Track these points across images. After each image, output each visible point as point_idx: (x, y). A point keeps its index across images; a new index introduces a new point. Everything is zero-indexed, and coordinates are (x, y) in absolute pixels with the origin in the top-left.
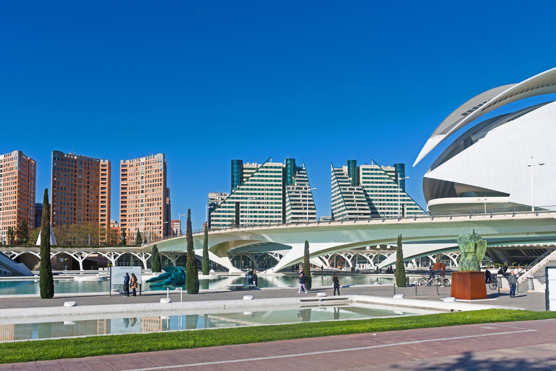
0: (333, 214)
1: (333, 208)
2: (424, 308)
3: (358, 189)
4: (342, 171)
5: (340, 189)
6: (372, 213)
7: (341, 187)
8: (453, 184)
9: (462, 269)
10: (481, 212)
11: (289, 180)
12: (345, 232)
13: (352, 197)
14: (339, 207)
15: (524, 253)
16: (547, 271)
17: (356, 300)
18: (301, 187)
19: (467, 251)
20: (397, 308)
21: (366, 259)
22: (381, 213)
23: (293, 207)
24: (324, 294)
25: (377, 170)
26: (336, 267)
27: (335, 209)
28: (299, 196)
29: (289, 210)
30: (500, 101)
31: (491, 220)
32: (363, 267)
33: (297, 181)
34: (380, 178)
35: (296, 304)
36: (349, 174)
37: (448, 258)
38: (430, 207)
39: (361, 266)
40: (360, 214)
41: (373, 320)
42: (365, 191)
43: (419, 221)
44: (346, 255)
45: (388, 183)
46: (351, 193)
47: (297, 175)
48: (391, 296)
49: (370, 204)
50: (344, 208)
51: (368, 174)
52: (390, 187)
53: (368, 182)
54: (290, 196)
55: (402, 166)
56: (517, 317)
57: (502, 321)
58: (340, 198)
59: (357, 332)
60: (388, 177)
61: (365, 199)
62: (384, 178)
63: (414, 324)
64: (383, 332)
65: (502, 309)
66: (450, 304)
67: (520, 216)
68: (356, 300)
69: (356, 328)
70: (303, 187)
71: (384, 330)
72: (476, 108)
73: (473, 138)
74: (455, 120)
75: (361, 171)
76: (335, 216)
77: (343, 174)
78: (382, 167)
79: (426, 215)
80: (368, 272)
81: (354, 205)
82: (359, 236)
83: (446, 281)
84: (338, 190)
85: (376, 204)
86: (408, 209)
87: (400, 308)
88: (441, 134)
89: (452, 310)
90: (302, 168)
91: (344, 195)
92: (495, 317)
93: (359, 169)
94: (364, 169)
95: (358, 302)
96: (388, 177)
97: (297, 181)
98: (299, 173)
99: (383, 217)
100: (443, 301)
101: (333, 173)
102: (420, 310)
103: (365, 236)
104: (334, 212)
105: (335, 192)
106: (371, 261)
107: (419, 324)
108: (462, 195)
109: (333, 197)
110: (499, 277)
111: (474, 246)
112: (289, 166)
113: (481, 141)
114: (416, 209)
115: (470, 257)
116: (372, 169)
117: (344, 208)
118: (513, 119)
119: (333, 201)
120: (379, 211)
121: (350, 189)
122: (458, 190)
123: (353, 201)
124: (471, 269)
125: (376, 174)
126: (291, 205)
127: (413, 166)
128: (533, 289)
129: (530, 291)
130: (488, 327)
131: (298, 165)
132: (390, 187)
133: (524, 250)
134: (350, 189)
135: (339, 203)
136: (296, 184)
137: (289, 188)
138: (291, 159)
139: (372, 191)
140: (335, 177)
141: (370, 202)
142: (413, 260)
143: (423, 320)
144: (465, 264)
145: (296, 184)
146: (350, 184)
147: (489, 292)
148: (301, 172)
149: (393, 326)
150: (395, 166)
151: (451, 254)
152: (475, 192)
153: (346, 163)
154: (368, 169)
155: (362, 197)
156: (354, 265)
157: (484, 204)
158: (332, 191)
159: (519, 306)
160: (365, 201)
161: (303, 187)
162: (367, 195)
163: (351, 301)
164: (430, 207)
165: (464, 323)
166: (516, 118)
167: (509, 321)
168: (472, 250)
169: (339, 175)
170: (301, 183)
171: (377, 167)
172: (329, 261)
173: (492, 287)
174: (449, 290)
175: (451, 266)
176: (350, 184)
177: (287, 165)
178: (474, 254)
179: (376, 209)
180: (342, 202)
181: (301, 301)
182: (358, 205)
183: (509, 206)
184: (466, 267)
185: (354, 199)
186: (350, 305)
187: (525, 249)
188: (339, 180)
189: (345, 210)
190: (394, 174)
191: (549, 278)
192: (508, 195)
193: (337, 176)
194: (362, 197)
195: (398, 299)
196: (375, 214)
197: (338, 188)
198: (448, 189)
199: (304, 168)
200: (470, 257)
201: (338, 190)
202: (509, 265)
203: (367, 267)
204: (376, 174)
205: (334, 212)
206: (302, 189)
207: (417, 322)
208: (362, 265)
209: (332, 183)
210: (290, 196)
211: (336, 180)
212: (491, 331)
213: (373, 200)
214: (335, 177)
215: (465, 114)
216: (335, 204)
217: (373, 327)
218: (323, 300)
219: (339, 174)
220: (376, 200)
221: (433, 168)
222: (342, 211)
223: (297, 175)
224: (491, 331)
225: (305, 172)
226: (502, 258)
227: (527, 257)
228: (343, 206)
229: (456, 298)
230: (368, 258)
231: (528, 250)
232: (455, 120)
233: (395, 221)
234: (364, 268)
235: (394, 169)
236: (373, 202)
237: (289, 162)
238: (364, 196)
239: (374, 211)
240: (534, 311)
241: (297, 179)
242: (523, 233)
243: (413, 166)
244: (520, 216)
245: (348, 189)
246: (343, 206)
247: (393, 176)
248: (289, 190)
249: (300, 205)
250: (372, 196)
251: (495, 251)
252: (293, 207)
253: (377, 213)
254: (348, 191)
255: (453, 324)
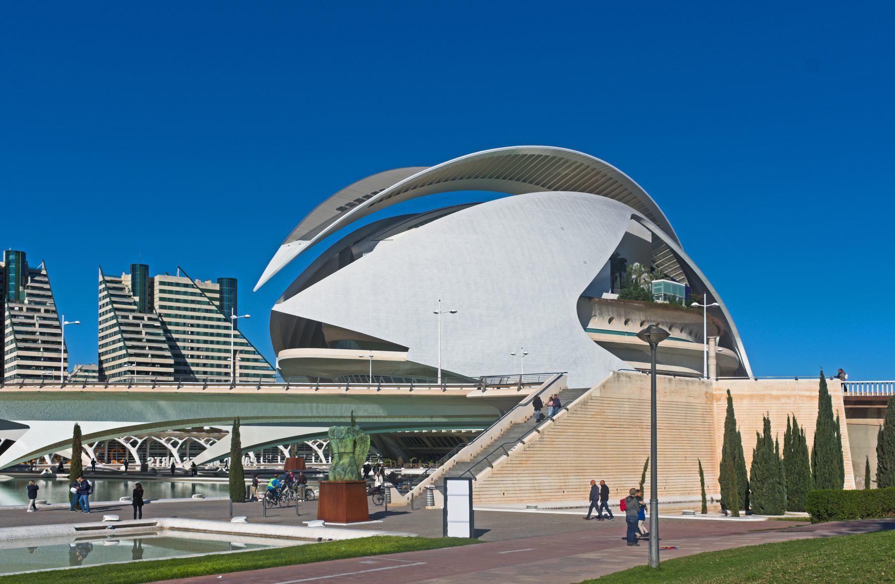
0: (101, 363)
1: (101, 351)
2: (279, 537)
3: (149, 319)
4: (120, 282)
5: (116, 317)
6: (176, 364)
7: (117, 313)
8: (319, 325)
9: (335, 478)
10: (362, 378)
11: (12, 292)
12: (137, 405)
13: (139, 333)
14: (114, 350)
15: (427, 442)
16: (445, 483)
17: (170, 526)
18: (37, 307)
19: (342, 450)
20: (237, 538)
21: (165, 448)
22: (193, 364)
23: (21, 345)
24: (116, 518)
25: (186, 286)
26: (109, 462)
27: (106, 353)
28: (34, 325)
29: (11, 351)
30: (398, 193)
31: (378, 395)
32: (161, 462)
33: (29, 295)
34: (193, 302)
35: (68, 535)
36: (134, 290)
37: (310, 449)
38: (280, 362)
39: (158, 461)
40: (154, 365)
41: (209, 558)
42: (163, 323)
43: (265, 390)
44: (128, 440)
45: (207, 311)
46: (138, 325)
47: (29, 284)
48: (228, 519)
49: (173, 348)
50: (124, 352)
51: (171, 292)
52: (210, 319)
53: (171, 308)
54: (13, 324)
55: (233, 282)
56: (406, 546)
57: (386, 553)
58: (115, 333)
59: (195, 574)
60: (206, 300)
61: (164, 339)
62: (199, 302)
63: (271, 561)
64: (231, 574)
65: (387, 537)
66: (316, 531)
67: (421, 390)
68: (170, 526)
69: (191, 569)
70: (42, 309)
71: (231, 570)
72: (360, 201)
73: (355, 250)
74: (327, 217)
75: (157, 287)
76: (105, 365)
77: (122, 289)
78: (197, 281)
79: (273, 373)
80: (173, 472)
81: (143, 348)
82: (160, 411)
83: (307, 492)
84: (112, 318)
85: (184, 348)
86: (243, 360)
87: (242, 537)
88: (304, 238)
89: (320, 539)
90: (40, 270)
91: (123, 328)
92: (378, 547)
93: (152, 282)
94: (162, 283)
95: (172, 529)
96: (206, 300)
97: (29, 295)
98: (32, 281)
99: (204, 380)
100: (306, 525)
101: (103, 286)
102: (214, 535)
103: (172, 412)
104: (103, 358)
105: (106, 320)
106: (174, 451)
107: (278, 561)
108: (334, 345)
109: (102, 330)
110: (387, 487)
111: (352, 443)
112: (13, 266)
113: (366, 257)
114: (256, 360)
115: (346, 460)
116: (178, 285)
117: (124, 352)
118: (416, 226)
119: (103, 338)
120: (189, 361)
121: (134, 318)
122: (329, 337)
123: (140, 340)
124: (347, 478)
125: (185, 293)
126: (17, 340)
127: (255, 290)
128: (433, 504)
129: (430, 507)
130: (368, 561)
131: (31, 265)
132: (210, 319)
133: (428, 438)
134: (134, 318)
135: (114, 342)
136: (26, 302)
137: (13, 309)
138: (17, 253)
139: (177, 324)
140: (106, 293)
141: (172, 343)
142: (251, 454)
143: (282, 554)
144: (339, 469)
145: (26, 302)
146: (135, 307)
147: (372, 510)
148: (37, 278)
149: (244, 564)
150: (220, 281)
151: (315, 442)
152: (356, 341)
153: (129, 269)
154: (170, 284)
155: (159, 335)
156: (143, 459)
157: (369, 361)
158: (100, 319)
159: (411, 532)
160: (164, 342)
161: (42, 309)
162: (167, 331)
163: (162, 529)
164: (280, 362)
165: (337, 558)
166: (422, 224)
167: (394, 552)
168: (349, 449)
169: (115, 291)
170: (37, 300)
171: (186, 280)
172: (95, 451)
173: (377, 502)
174: (314, 508)
175: (313, 462)
176: (135, 307)
177: (8, 263)
178: (351, 455)
179: (183, 356)
180: (119, 341)
181: (77, 529)
182: (150, 348)
183: (408, 367)
184: (340, 474)
185: (143, 336)
186: (159, 535)
187: (430, 436)
188: (114, 299)
189: (124, 356)
190: (217, 296)
191: (448, 493)
192: (405, 349)
193: (111, 292)
194: (159, 335)
195: (238, 524)
196: (183, 372)
197: (112, 314)
198: (312, 332)
199: (44, 272)
200: (346, 460)
201: (112, 318)
202: (405, 462)
203: (166, 463)
204: (185, 293)
205: (103, 358)
206: (39, 310)
207: (275, 558)
208: (158, 459)
209: (100, 303)
210: (13, 324)
211: (108, 300)
212: (372, 567)
213: (178, 340)
214: (106, 293)
215: (343, 210)
216: (106, 345)
217: (217, 567)
218: (114, 527)
219: (114, 288)
220: (184, 340)
221: (288, 295)
222: (120, 357)
223: (29, 284)
224: (372, 567)
225: (46, 279)
226: (395, 450)
227: (432, 448)
228: (121, 348)
229: (326, 521)
230: (169, 446)
231: (433, 438)
232: (327, 217)
233: (225, 389)
234: (163, 465)
235: (217, 287)
236: (179, 344)
237: (12, 257)
238: (161, 331)
239: (179, 360)
240: (429, 537)
241: (30, 291)
242: (427, 417)
243: (255, 290)
244: (421, 390)
245: (131, 317)
246: (121, 348)
247: (215, 299)
248: (13, 313)
249: (35, 341)
250: (177, 332)
251: (384, 438)
252: (21, 345)
253: (186, 364)
254: (131, 320)
255: (324, 559)
